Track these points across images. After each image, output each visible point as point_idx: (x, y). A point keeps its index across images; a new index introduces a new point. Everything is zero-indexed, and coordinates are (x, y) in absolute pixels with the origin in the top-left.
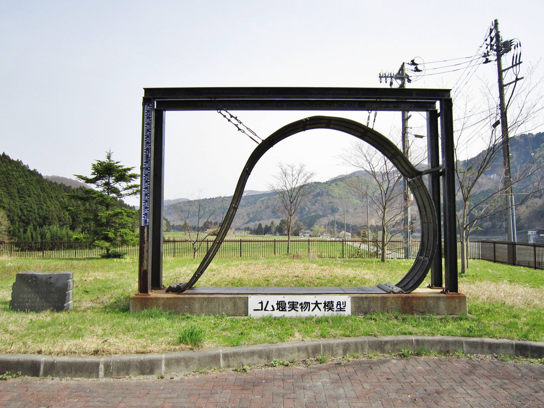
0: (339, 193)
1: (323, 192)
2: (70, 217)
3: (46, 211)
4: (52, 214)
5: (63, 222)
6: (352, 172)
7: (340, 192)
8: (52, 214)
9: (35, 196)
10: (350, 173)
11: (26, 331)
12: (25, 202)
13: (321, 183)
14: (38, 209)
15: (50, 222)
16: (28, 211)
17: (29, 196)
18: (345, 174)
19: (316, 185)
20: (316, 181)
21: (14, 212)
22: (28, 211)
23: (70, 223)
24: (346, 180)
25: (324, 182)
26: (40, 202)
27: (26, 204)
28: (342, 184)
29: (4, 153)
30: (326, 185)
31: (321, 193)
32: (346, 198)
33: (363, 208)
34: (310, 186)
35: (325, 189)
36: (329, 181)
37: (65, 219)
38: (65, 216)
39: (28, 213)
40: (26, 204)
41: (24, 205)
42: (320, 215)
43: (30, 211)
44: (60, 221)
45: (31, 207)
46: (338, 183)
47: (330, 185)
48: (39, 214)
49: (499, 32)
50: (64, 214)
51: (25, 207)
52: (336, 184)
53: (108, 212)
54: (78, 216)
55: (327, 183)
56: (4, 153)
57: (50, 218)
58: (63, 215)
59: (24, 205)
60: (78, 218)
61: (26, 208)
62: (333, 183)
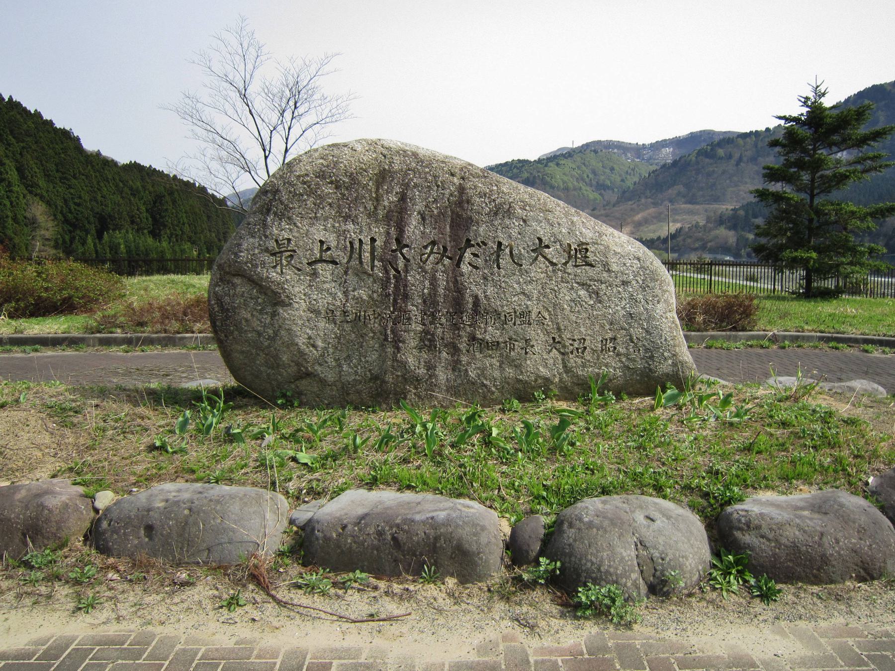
0: (562, 179)
1: (534, 177)
2: (149, 216)
3: (102, 205)
4: (119, 210)
5: (137, 224)
6: (585, 143)
7: (565, 178)
8: (119, 210)
9: (83, 177)
10: (580, 145)
11: (154, 471)
12: (70, 187)
13: (530, 162)
14: (91, 200)
15: (117, 225)
16: (75, 204)
17: (74, 177)
18: (570, 146)
19: (521, 165)
20: (521, 158)
21: (56, 207)
22: (75, 204)
23: (149, 227)
24: (575, 156)
25: (535, 161)
26: (92, 187)
27: (72, 191)
28: (569, 163)
29: (11, 96)
30: (539, 165)
31: (531, 179)
32: (575, 189)
33: (607, 207)
34: (511, 167)
35: (538, 172)
36: (544, 159)
37: (141, 220)
38: (140, 212)
39: (76, 207)
40: (72, 191)
41: (69, 192)
42: (872, 217)
43: (79, 205)
44: (133, 222)
45: (80, 197)
46: (562, 162)
47: (546, 166)
48: (92, 210)
49: (150, 166)
50: (138, 210)
51: (70, 196)
52: (558, 164)
53: (41, 219)
54: (163, 214)
55: (539, 161)
56: (11, 96)
57: (117, 216)
58: (138, 212)
59: (69, 192)
60: (162, 217)
61: (72, 198)
62: (552, 161)
